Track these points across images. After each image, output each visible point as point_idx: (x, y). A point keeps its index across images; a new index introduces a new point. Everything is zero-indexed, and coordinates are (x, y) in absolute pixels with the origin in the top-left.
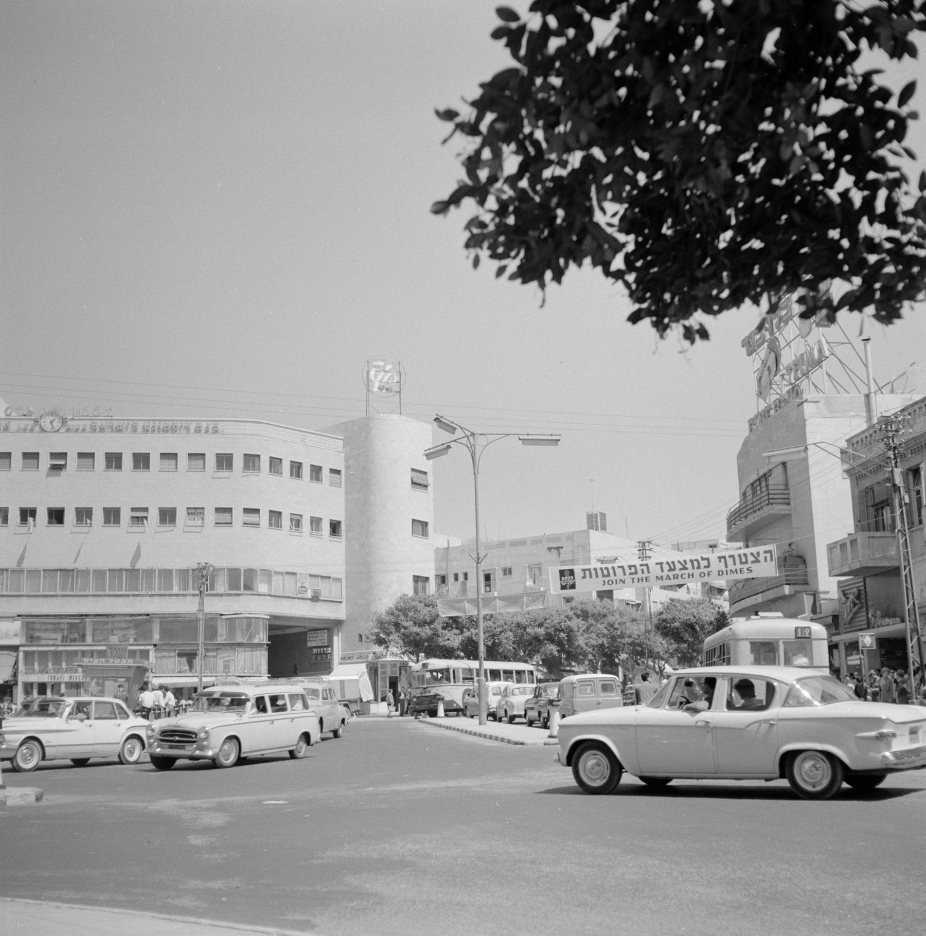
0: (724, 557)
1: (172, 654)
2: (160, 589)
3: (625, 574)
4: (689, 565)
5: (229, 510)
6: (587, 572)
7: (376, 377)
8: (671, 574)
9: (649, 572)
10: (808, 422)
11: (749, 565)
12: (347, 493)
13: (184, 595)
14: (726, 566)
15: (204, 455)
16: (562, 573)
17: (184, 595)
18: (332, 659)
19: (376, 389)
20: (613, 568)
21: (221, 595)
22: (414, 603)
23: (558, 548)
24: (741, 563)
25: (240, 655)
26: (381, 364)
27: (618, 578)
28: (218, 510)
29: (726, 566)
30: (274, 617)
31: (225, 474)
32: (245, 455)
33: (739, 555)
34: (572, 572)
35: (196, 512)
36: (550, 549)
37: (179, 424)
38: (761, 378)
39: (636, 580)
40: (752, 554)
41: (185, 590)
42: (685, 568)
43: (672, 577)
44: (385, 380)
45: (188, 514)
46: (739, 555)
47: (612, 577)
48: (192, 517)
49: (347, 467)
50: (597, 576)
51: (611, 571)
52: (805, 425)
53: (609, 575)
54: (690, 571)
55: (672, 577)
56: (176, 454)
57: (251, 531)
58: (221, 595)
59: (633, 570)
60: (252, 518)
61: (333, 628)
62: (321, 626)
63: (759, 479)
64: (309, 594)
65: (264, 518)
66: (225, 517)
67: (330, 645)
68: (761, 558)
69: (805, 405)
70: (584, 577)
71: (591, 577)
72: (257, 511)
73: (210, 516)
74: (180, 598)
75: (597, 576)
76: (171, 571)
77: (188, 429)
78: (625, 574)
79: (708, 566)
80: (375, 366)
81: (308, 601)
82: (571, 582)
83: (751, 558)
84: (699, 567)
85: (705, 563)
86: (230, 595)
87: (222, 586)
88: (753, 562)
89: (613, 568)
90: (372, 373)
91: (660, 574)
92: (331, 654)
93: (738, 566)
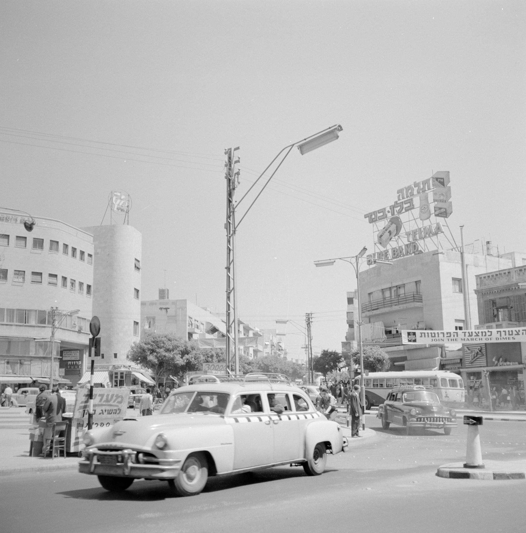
0: (500, 332)
1: (3, 362)
2: (7, 321)
3: (444, 336)
4: (480, 334)
5: (40, 274)
6: (423, 334)
7: (116, 201)
8: (470, 338)
9: (457, 336)
10: (440, 264)
11: (514, 336)
12: (95, 269)
13: (12, 325)
14: (501, 336)
15: (26, 238)
16: (409, 334)
17: (12, 325)
18: (82, 368)
19: (115, 209)
20: (438, 333)
21: (34, 326)
22: (163, 339)
23: (166, 309)
24: (509, 335)
25: (45, 364)
26: (119, 194)
27: (440, 338)
28: (34, 273)
29: (501, 336)
30: (62, 342)
31: (38, 251)
32: (51, 241)
33: (509, 331)
34: (414, 334)
35: (20, 273)
36: (161, 309)
37: (11, 216)
38: (381, 236)
39: (450, 340)
40: (516, 331)
41: (10, 321)
42: (477, 335)
43: (470, 339)
44: (121, 204)
45: (15, 274)
46: (509, 331)
47: (437, 338)
48: (16, 276)
49: (96, 253)
50: (428, 336)
51: (437, 335)
52: (439, 264)
53: (435, 336)
54: (480, 337)
55: (470, 339)
56: (8, 236)
57: (52, 287)
58: (34, 326)
59: (449, 335)
60: (53, 280)
61: (83, 350)
62: (76, 348)
63: (390, 288)
64: (77, 329)
65: (60, 280)
66: (38, 278)
67: (81, 359)
68: (521, 333)
69: (439, 255)
70: (421, 336)
71: (425, 336)
72: (56, 276)
73: (29, 276)
74: (8, 326)
75: (428, 336)
76: (13, 310)
77: (16, 220)
78: (444, 336)
79: (491, 335)
80: (116, 195)
81: (76, 333)
82: (414, 339)
83: (514, 333)
84: (485, 335)
85: (490, 334)
86: (39, 327)
87: (33, 322)
88: (516, 335)
89: (438, 333)
90: (114, 198)
91: (463, 337)
92: (82, 365)
93: (507, 336)
